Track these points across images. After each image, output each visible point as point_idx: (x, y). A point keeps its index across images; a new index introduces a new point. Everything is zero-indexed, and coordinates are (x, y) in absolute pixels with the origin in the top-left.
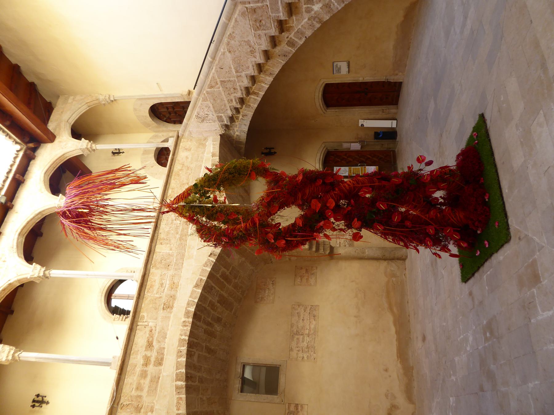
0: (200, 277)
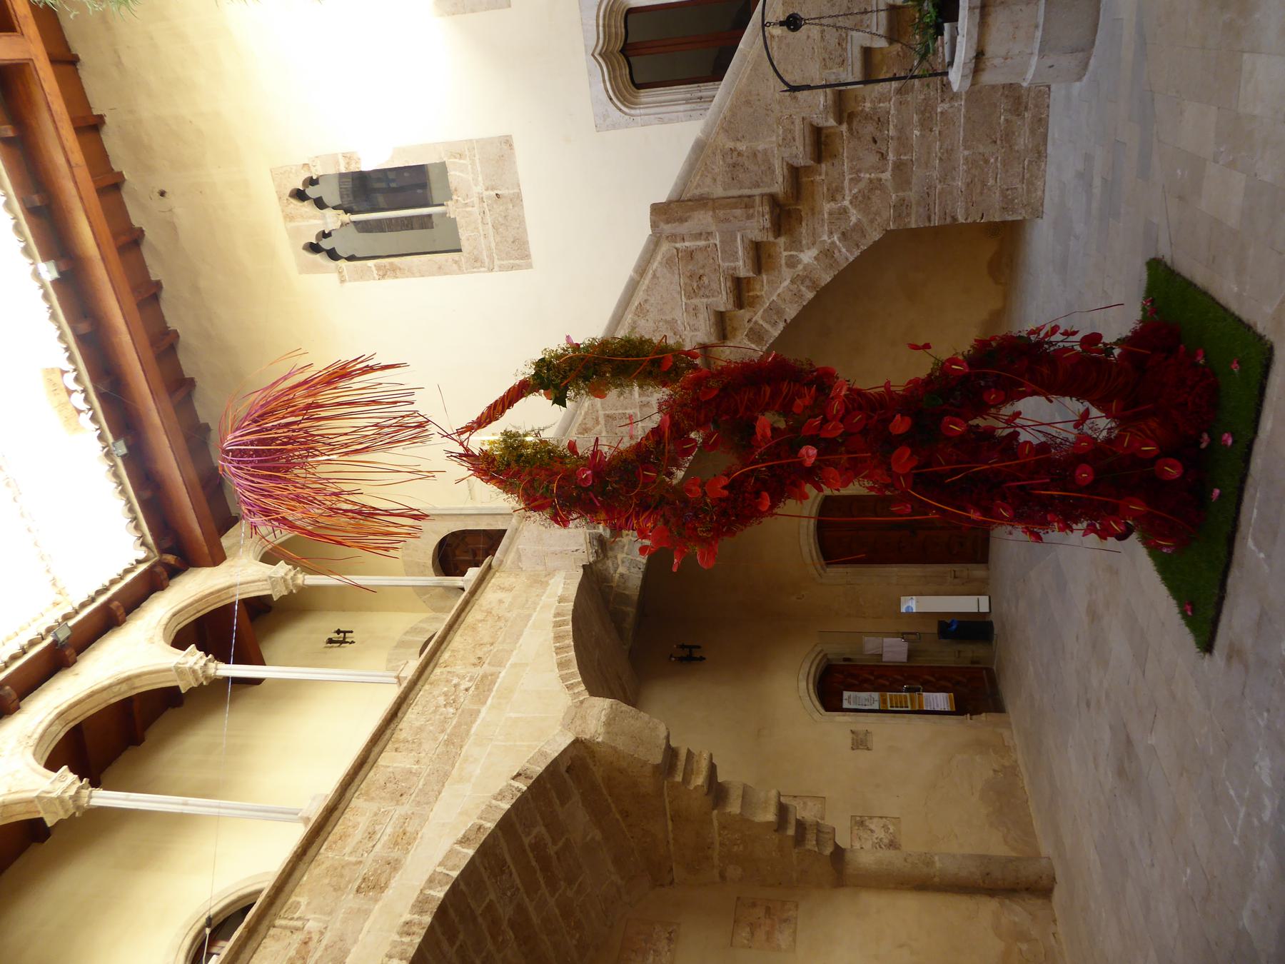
0: (477, 821)
